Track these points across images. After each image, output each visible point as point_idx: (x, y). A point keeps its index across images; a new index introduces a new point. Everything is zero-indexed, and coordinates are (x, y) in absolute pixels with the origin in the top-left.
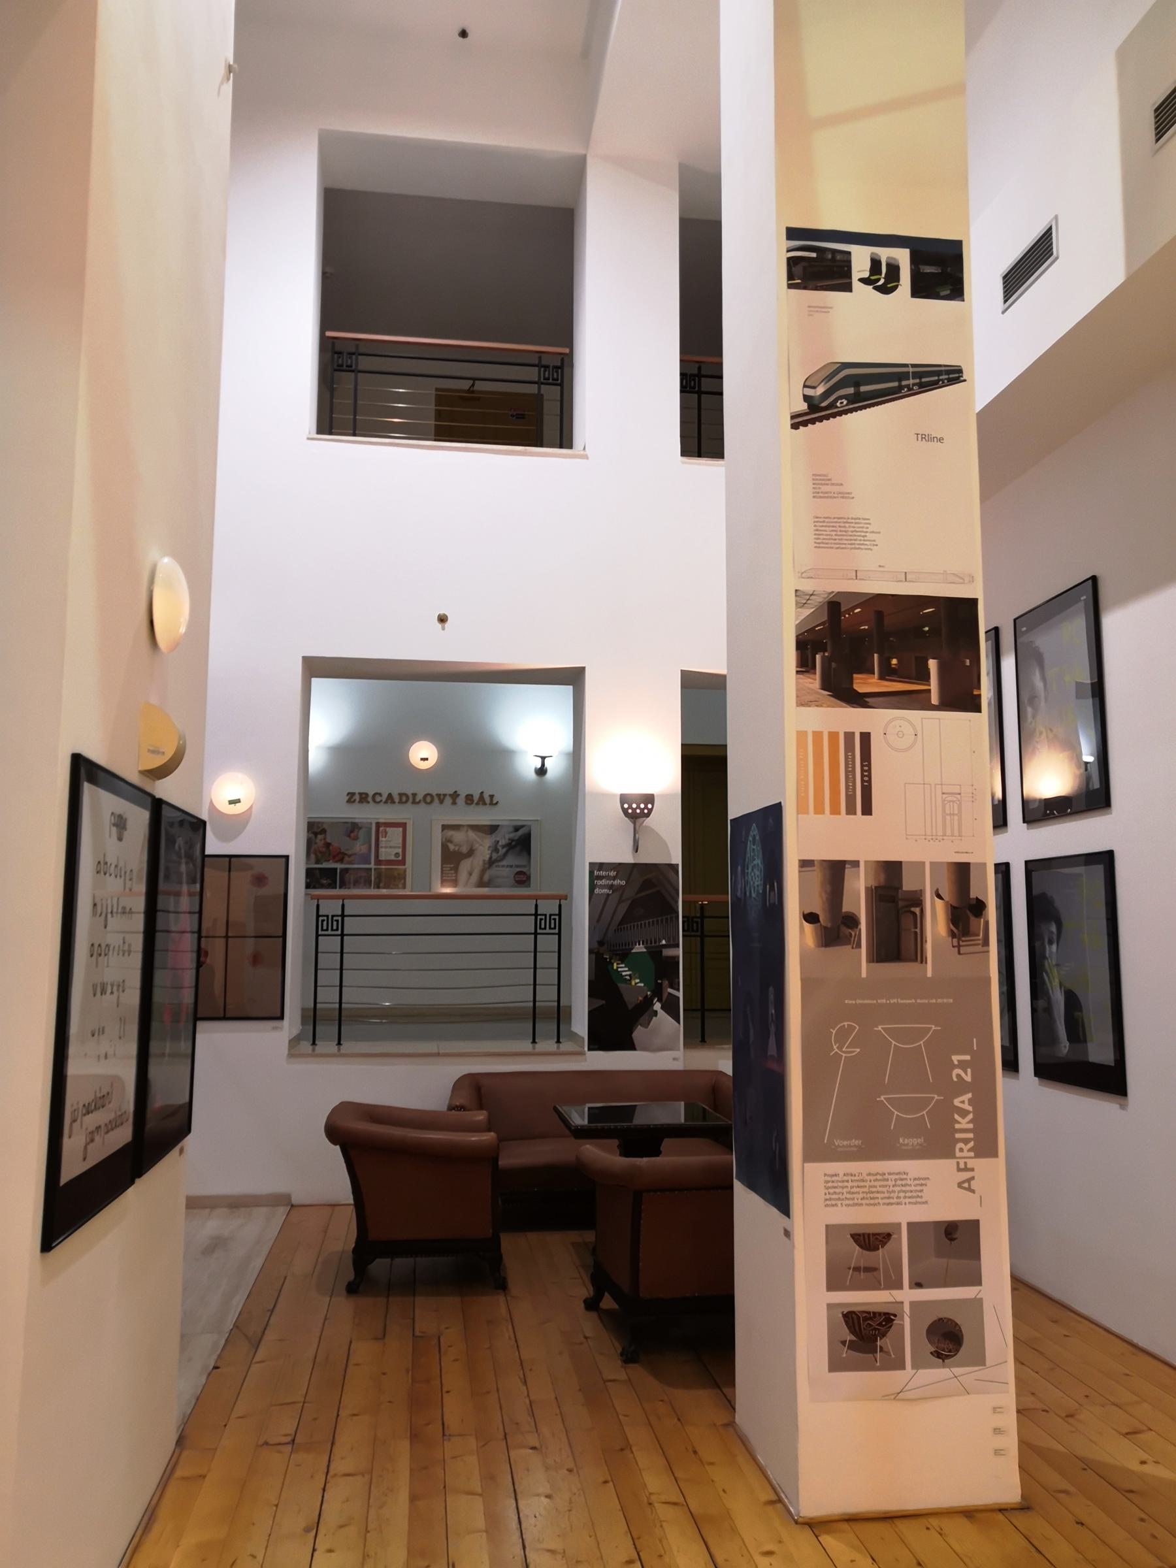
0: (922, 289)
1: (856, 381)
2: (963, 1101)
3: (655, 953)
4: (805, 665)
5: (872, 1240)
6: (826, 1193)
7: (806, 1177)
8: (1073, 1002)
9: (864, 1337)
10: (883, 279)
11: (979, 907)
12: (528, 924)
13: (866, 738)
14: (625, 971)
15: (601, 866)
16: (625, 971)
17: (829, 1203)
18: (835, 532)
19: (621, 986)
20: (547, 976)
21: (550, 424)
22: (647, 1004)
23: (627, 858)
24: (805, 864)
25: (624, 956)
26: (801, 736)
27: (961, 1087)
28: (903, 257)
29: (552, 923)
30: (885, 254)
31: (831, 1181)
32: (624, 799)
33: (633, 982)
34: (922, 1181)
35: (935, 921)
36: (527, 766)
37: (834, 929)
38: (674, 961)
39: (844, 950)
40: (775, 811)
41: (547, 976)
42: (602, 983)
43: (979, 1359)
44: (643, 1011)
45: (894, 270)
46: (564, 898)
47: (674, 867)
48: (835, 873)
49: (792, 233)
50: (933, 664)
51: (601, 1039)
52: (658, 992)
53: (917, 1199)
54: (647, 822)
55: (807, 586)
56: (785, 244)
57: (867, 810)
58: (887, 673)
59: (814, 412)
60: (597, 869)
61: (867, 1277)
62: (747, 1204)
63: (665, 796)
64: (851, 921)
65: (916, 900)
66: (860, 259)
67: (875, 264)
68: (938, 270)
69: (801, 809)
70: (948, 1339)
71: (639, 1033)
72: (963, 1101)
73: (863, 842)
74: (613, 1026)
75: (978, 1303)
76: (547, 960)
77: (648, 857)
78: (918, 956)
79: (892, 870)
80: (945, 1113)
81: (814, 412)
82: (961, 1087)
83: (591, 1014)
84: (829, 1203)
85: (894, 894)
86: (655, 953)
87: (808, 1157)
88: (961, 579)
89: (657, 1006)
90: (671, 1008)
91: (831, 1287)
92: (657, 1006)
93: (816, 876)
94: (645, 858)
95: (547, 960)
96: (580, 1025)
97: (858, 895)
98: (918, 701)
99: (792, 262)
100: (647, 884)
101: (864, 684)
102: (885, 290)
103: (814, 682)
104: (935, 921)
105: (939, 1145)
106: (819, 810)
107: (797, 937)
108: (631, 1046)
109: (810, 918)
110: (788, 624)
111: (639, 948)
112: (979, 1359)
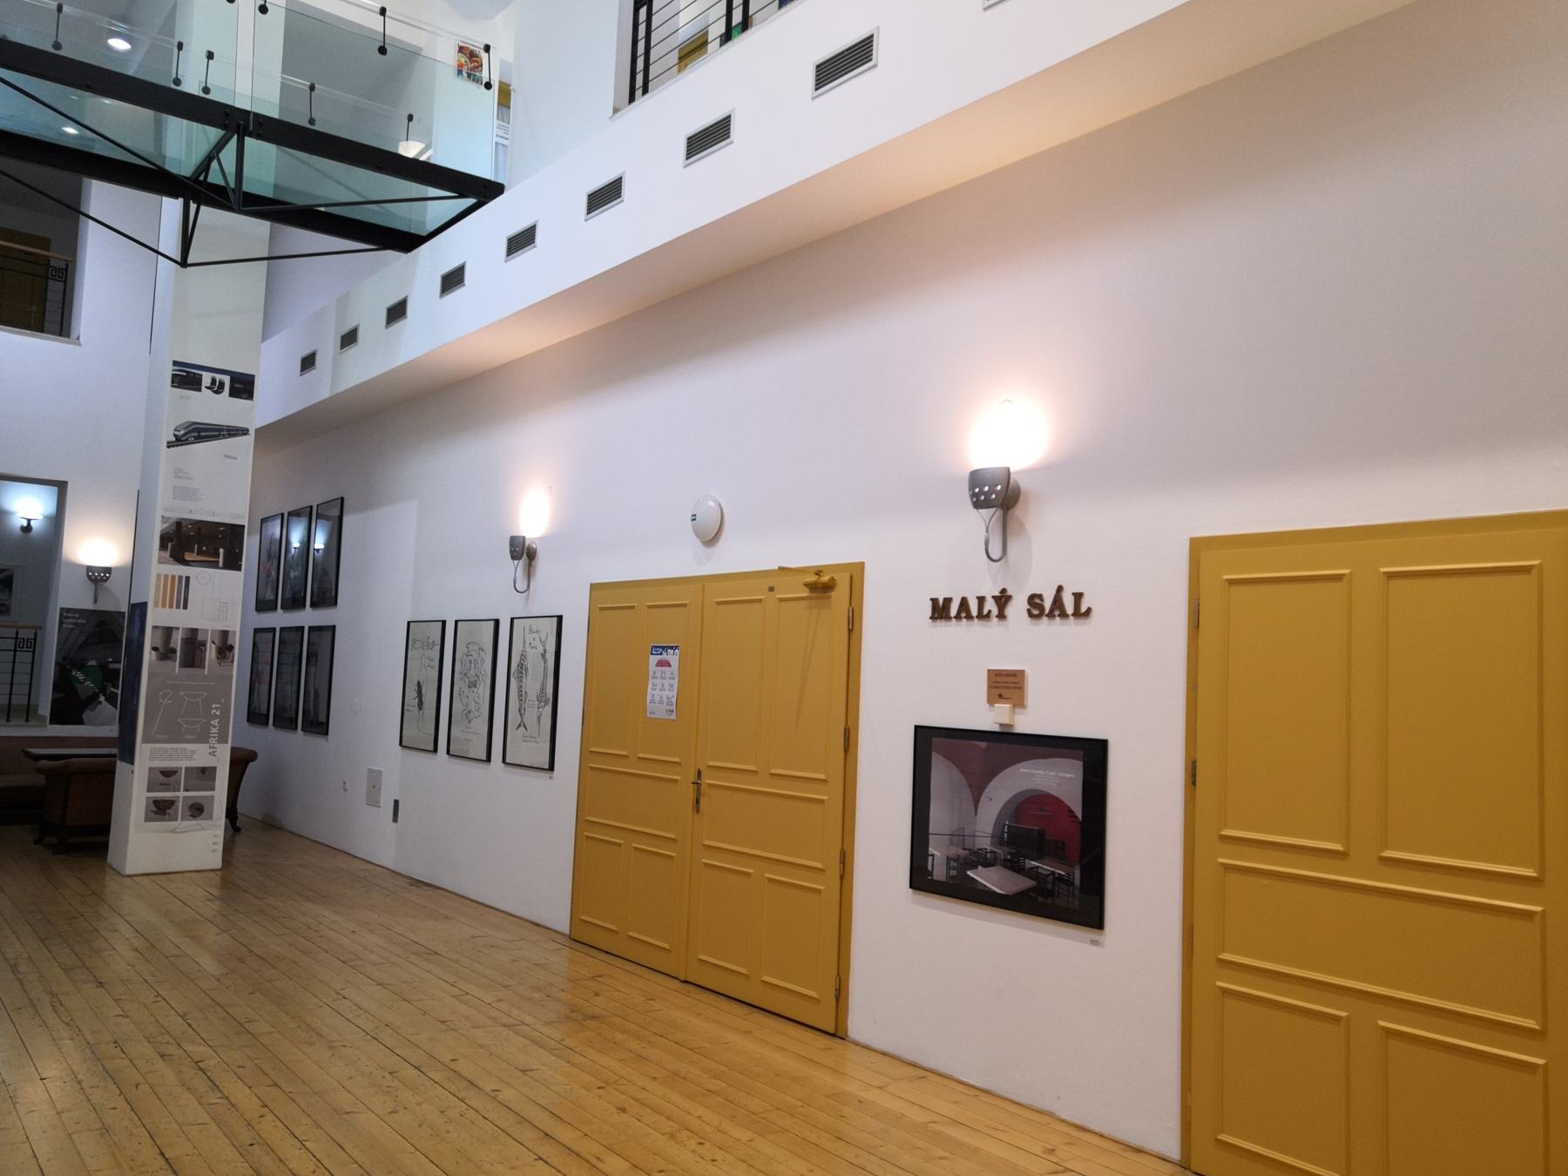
0: (234, 393)
1: (199, 430)
2: (215, 722)
3: (103, 666)
4: (163, 547)
5: (168, 773)
6: (147, 756)
7: (142, 750)
8: (316, 692)
9: (161, 809)
10: (217, 388)
11: (231, 648)
12: (10, 644)
13: (188, 579)
14: (80, 676)
15: (69, 610)
16: (80, 676)
17: (151, 759)
18: (183, 493)
19: (78, 687)
20: (22, 679)
21: (52, 315)
22: (95, 697)
23: (89, 606)
24: (155, 627)
25: (81, 666)
26: (159, 576)
27: (215, 716)
28: (227, 379)
29: (29, 644)
30: (218, 377)
31: (152, 751)
32: (89, 569)
33: (85, 683)
34: (193, 752)
35: (211, 652)
36: (18, 521)
37: (165, 653)
38: (117, 672)
39: (169, 662)
40: (145, 604)
41: (22, 679)
42: (63, 683)
43: (210, 817)
44: (92, 700)
45: (222, 384)
46: (39, 629)
47: (122, 614)
48: (168, 632)
49: (175, 363)
50: (221, 551)
51: (59, 716)
52: (103, 690)
53: (190, 758)
54: (107, 584)
55: (168, 514)
56: (171, 367)
57: (185, 607)
58: (200, 553)
59: (178, 441)
60: (65, 613)
61: (165, 787)
62: (121, 766)
63: (118, 569)
64: (174, 651)
65: (204, 644)
66: (207, 378)
67: (214, 381)
68: (243, 386)
69: (156, 605)
70: (197, 810)
71: (87, 715)
72: (215, 722)
73: (181, 620)
74: (68, 708)
75: (212, 797)
76: (23, 668)
77: (105, 605)
78: (202, 666)
79: (194, 631)
80: (208, 726)
81: (178, 441)
82: (215, 716)
83: (54, 702)
84: (151, 759)
85: (193, 643)
86: (103, 666)
87: (146, 740)
88: (237, 517)
89: (102, 698)
90: (111, 700)
91: (149, 790)
92: (102, 698)
93: (159, 633)
94: (101, 607)
95: (23, 668)
96: (45, 710)
97: (177, 641)
98: (215, 565)
99: (174, 376)
100: (101, 623)
101: (188, 556)
102: (217, 392)
103: (167, 554)
104: (211, 652)
105: (203, 737)
106: (164, 606)
107: (148, 656)
108: (81, 722)
109: (155, 649)
110: (158, 529)
111: (93, 663)
112: (210, 817)
